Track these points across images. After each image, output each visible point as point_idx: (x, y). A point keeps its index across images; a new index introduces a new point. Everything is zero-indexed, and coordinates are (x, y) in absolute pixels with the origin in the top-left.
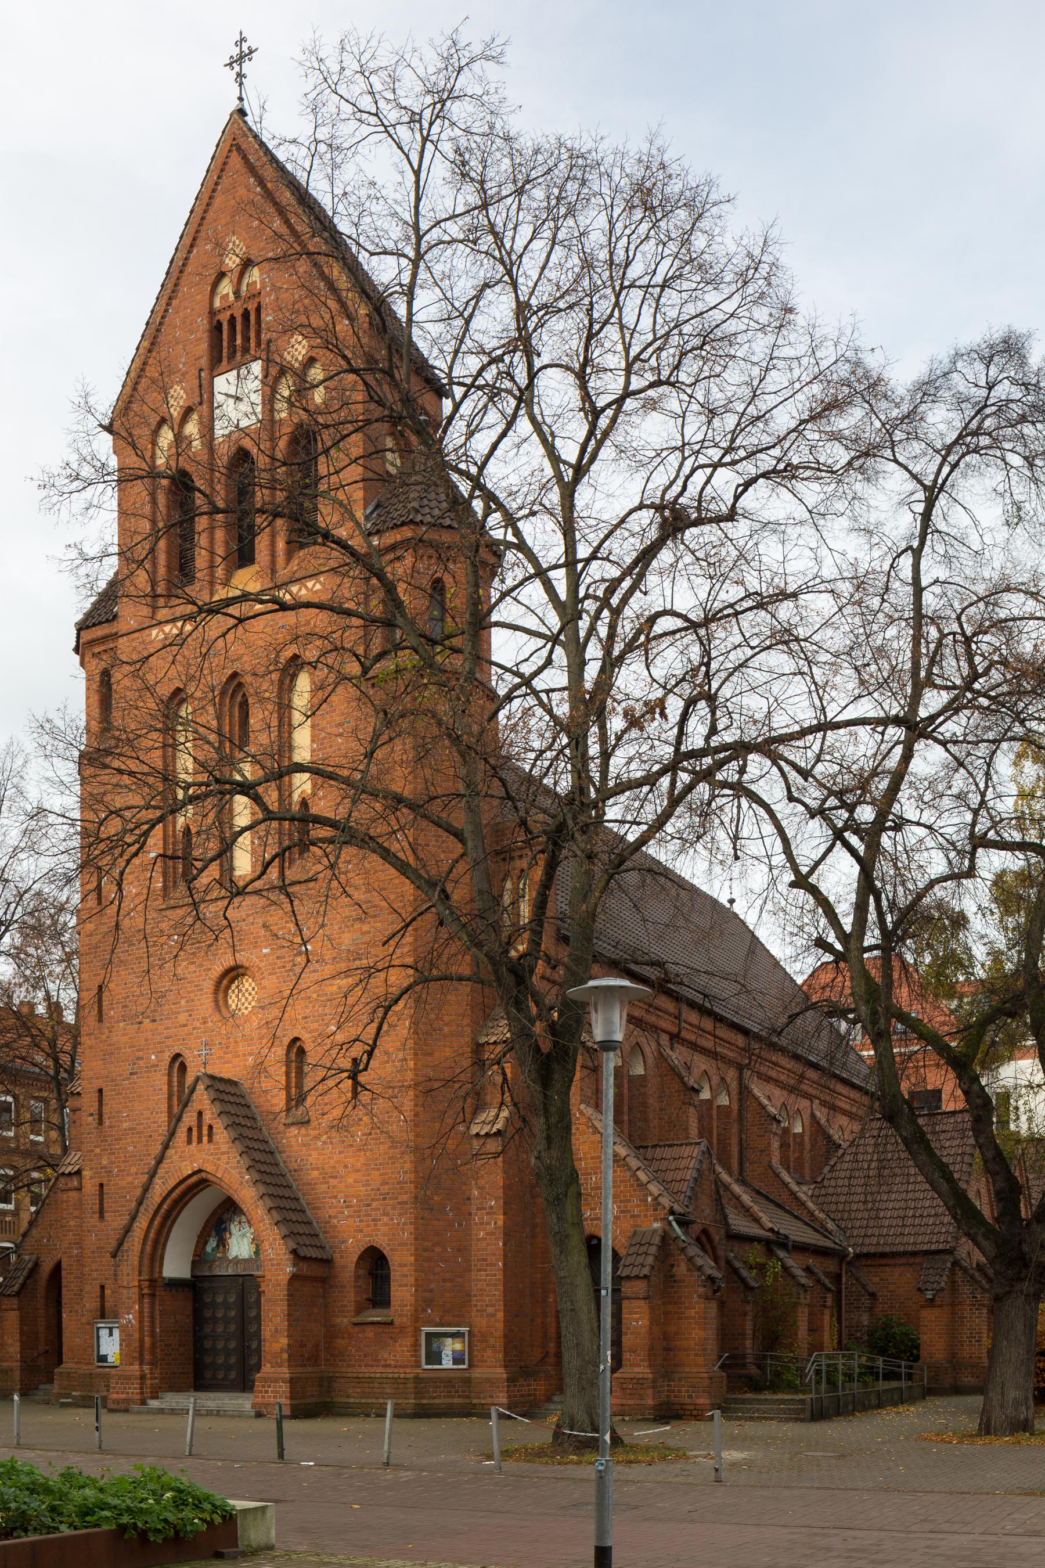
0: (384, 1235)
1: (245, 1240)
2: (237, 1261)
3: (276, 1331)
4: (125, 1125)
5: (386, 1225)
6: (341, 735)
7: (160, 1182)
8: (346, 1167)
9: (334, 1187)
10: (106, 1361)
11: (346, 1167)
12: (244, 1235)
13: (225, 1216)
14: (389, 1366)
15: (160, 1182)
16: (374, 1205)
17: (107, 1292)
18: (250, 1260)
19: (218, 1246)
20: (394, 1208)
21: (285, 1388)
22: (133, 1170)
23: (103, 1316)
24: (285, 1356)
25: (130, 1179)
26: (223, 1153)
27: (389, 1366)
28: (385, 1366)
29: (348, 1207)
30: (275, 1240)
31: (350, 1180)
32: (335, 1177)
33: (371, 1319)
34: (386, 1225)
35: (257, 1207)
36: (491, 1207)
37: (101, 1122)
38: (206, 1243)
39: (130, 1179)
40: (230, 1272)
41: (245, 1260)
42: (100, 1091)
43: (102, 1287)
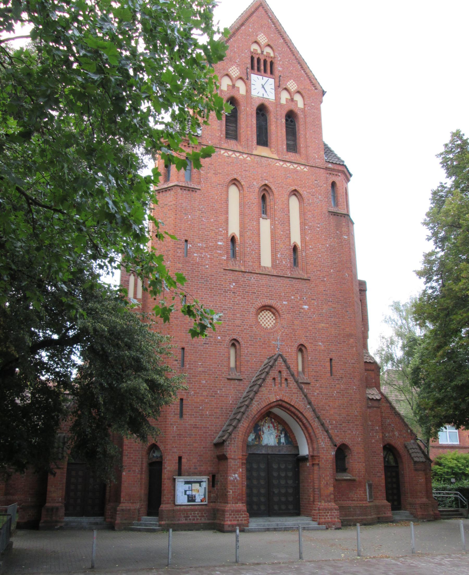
0: (349, 439)
1: (272, 436)
2: (267, 446)
3: (327, 484)
4: (200, 369)
5: (349, 434)
6: (319, 227)
7: (256, 403)
8: (329, 406)
9: (324, 414)
10: (194, 501)
11: (329, 406)
12: (271, 434)
13: (260, 423)
14: (354, 500)
15: (256, 403)
16: (344, 425)
17: (184, 460)
18: (275, 447)
19: (255, 438)
20: (353, 427)
21: (336, 513)
22: (205, 393)
23: (180, 474)
24: (332, 496)
25: (203, 398)
26: (294, 393)
27: (354, 500)
28: (352, 500)
29: (331, 424)
30: (325, 438)
31: (332, 412)
32: (324, 410)
33: (345, 478)
34: (349, 434)
35: (314, 421)
36: (377, 430)
37: (183, 365)
38: (248, 436)
39: (203, 398)
40: (263, 452)
41: (272, 447)
42: (183, 349)
43: (180, 458)
